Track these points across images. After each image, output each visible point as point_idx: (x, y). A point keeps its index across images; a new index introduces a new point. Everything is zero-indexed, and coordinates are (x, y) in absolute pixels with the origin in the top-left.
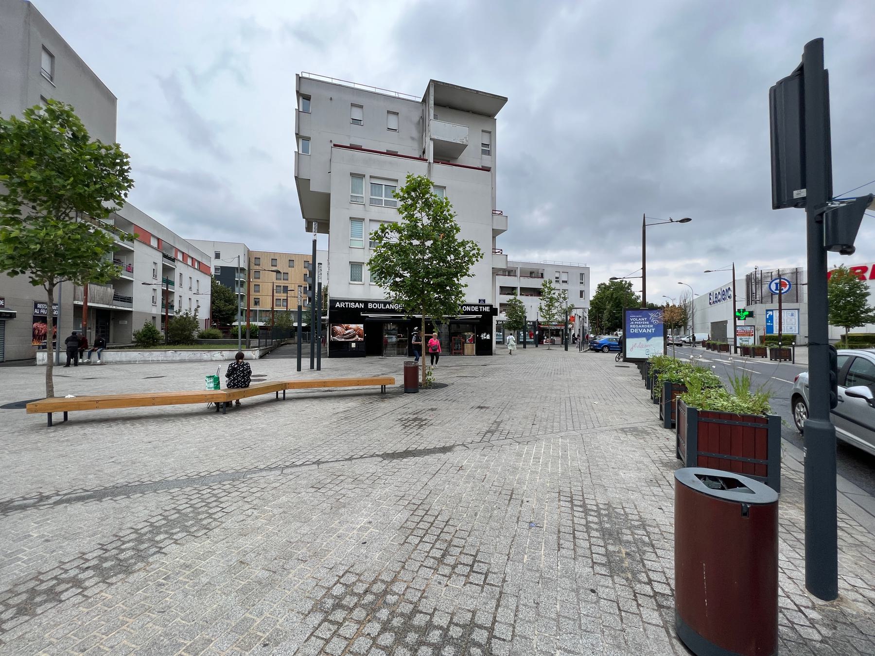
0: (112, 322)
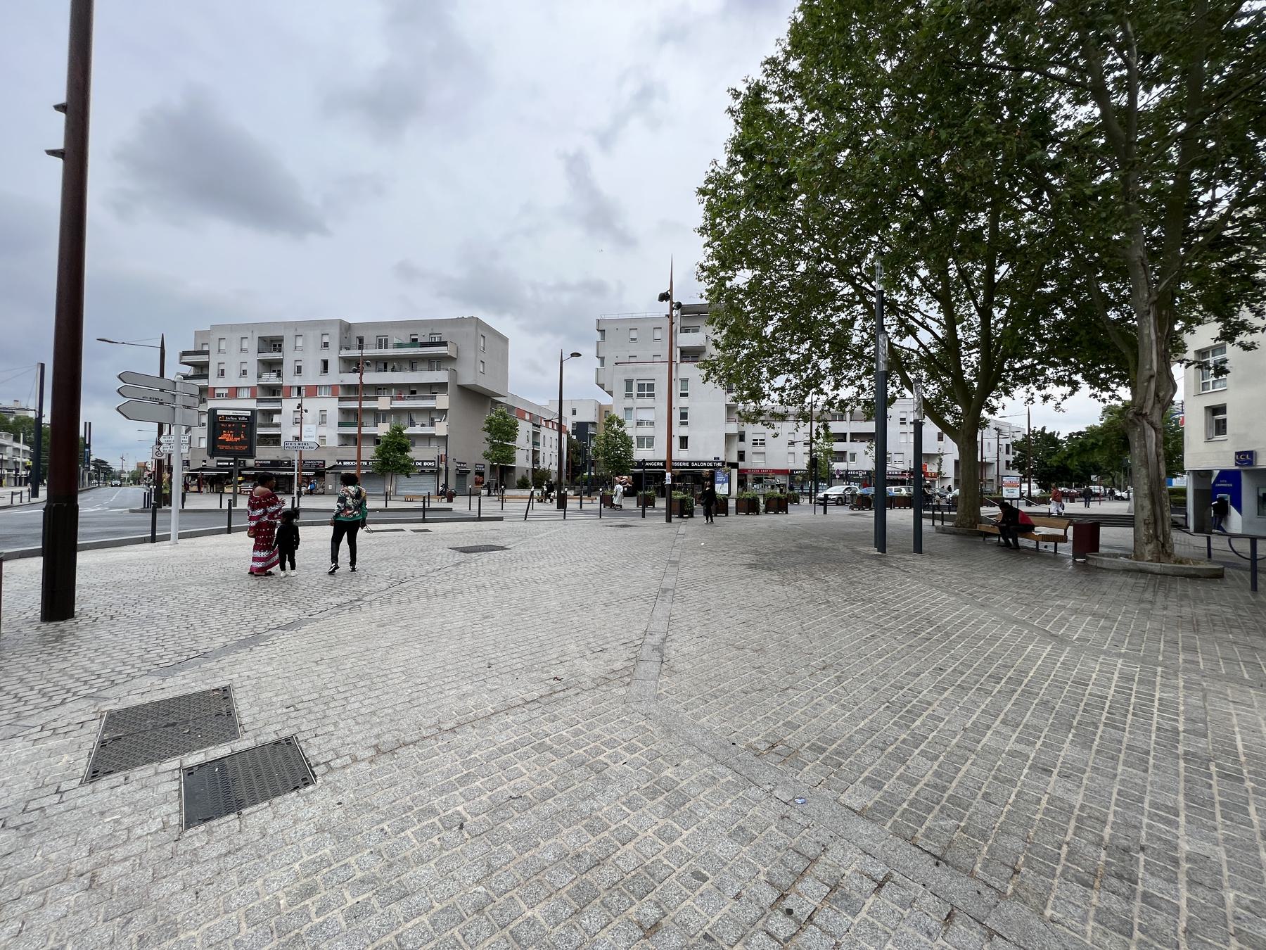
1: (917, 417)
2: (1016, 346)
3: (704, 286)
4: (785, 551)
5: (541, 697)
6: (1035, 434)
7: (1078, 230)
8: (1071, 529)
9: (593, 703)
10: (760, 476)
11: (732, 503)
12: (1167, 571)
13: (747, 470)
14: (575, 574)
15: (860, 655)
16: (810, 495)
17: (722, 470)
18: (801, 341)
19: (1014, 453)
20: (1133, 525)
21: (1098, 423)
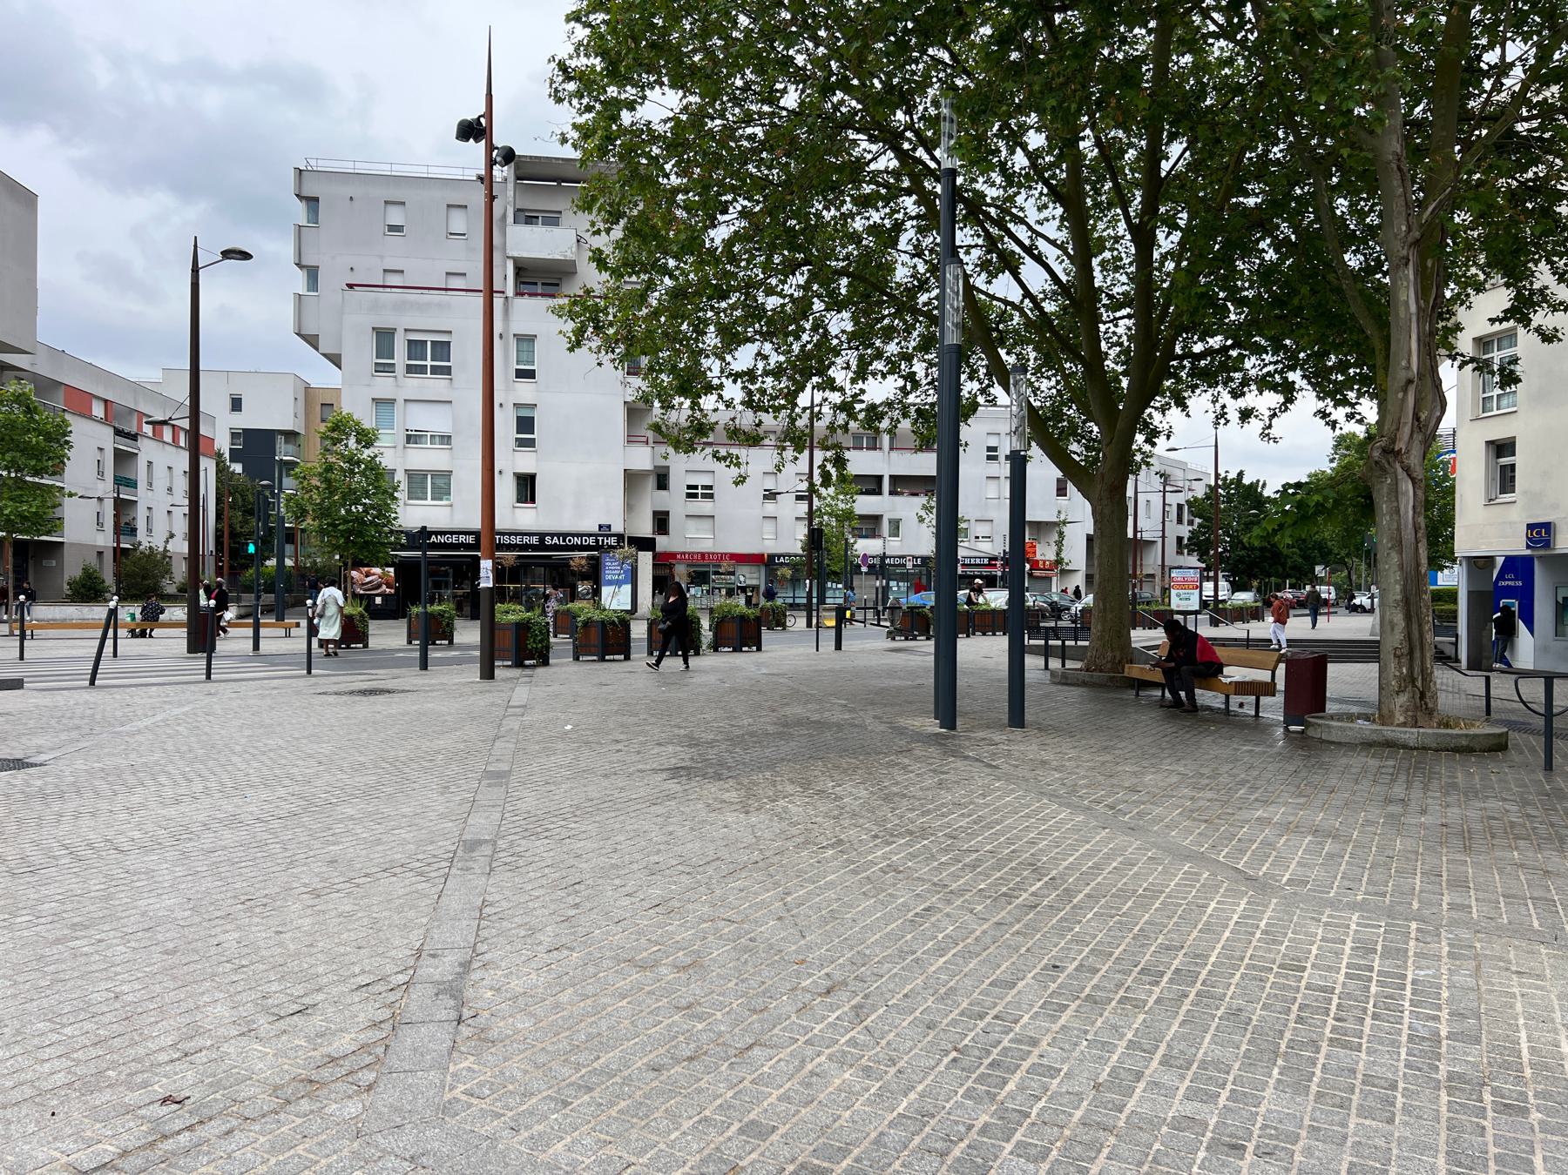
0: (31, 562)
1: (1017, 446)
2: (1196, 310)
3: (568, 116)
4: (752, 734)
5: (125, 1153)
6: (1226, 486)
7: (1301, 89)
8: (1281, 669)
9: (273, 1150)
10: (704, 569)
11: (639, 630)
12: (1430, 742)
13: (673, 555)
14: (233, 821)
15: (902, 955)
16: (808, 608)
17: (618, 554)
18: (791, 268)
19: (1191, 523)
20: (1377, 659)
21: (1327, 467)
